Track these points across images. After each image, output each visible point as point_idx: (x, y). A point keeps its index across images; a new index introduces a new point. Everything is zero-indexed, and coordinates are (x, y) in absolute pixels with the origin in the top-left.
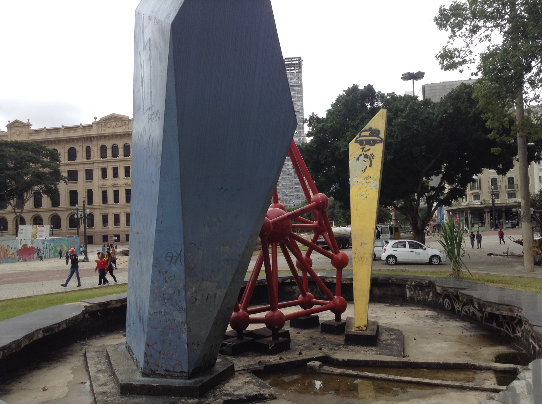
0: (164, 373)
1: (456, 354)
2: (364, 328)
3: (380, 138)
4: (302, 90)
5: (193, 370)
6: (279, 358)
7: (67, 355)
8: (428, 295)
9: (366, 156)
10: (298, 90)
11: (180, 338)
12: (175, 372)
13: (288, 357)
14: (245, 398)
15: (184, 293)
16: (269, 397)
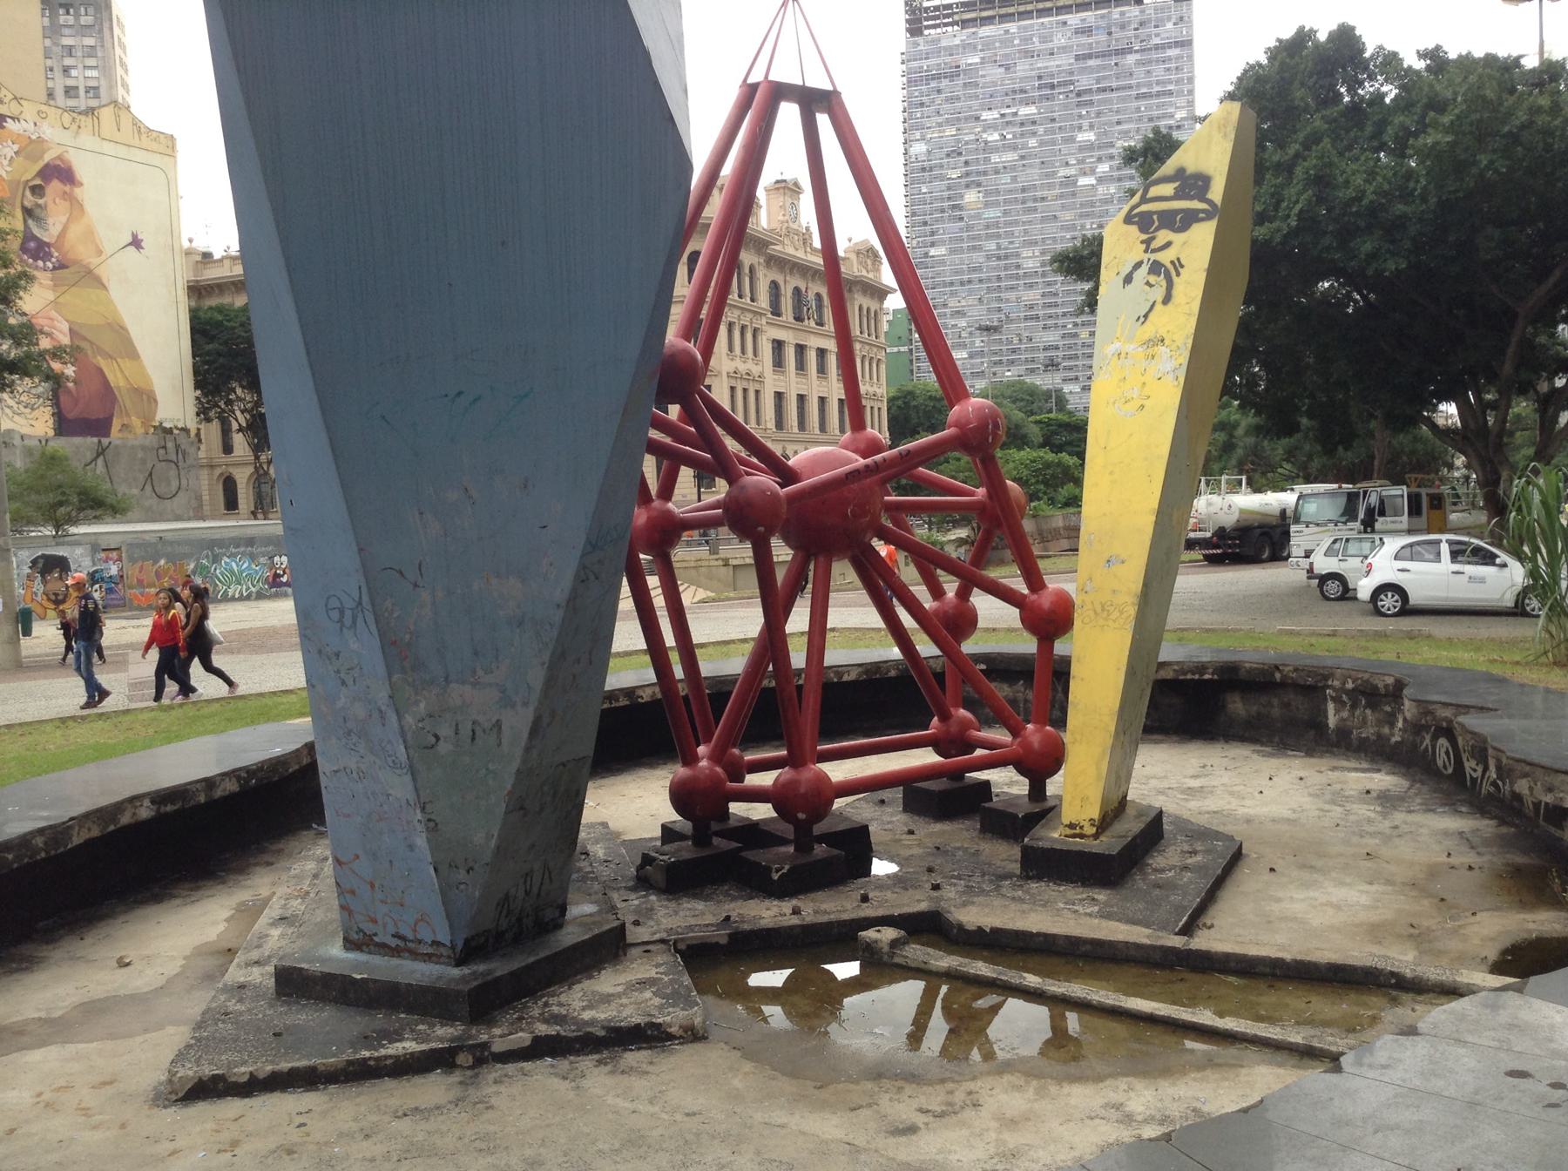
0: (393, 942)
1: (1376, 932)
2: (1090, 830)
3: (1210, 202)
4: (1190, 57)
5: (467, 941)
6: (788, 911)
7: (256, 865)
8: (1392, 725)
9: (1156, 268)
10: (1178, 58)
11: (411, 847)
12: (420, 942)
13: (824, 906)
14: (602, 1033)
15: (392, 717)
16: (681, 1032)
